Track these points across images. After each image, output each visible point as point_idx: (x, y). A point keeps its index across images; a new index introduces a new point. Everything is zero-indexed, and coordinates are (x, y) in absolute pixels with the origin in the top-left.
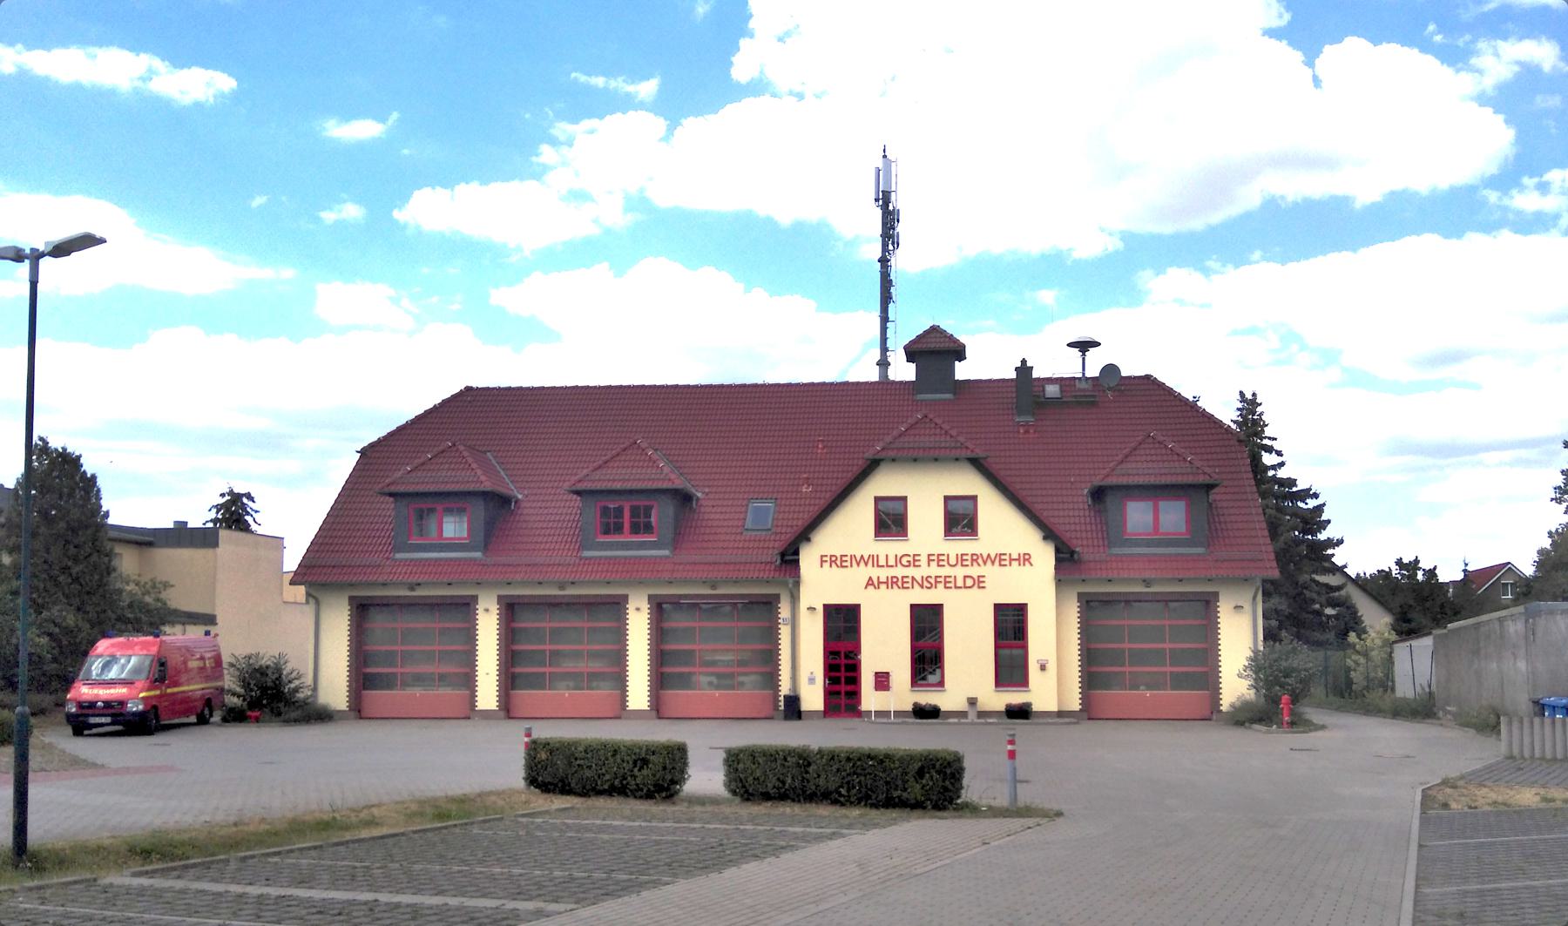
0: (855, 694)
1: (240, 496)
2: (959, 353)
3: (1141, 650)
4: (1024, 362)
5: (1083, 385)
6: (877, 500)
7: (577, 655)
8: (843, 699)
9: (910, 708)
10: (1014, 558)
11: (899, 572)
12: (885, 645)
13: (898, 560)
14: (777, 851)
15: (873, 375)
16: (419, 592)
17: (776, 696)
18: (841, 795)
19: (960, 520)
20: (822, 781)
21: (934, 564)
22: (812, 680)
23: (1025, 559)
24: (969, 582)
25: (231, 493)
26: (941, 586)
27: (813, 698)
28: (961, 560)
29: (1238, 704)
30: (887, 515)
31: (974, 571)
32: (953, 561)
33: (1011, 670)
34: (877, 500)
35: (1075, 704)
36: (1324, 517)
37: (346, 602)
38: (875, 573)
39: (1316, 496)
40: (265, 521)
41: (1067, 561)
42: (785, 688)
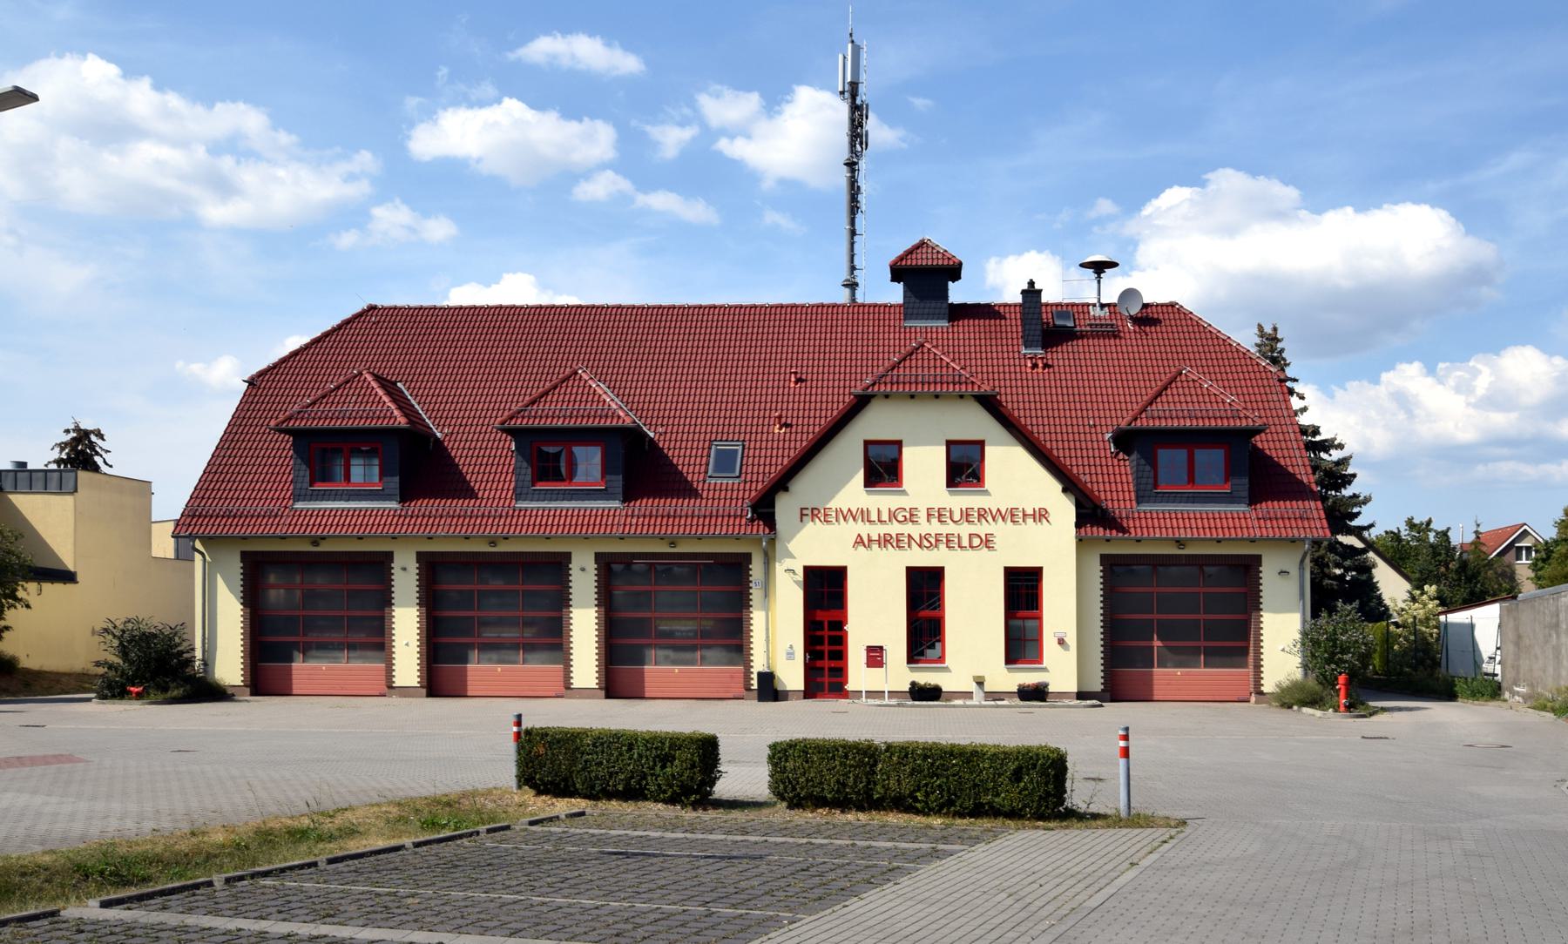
0: (840, 672)
1: (86, 433)
2: (954, 272)
3: (1166, 618)
4: (1031, 283)
5: (1097, 312)
6: (867, 443)
7: (500, 623)
8: (826, 679)
9: (906, 688)
10: (1028, 514)
11: (894, 529)
12: (875, 614)
13: (893, 515)
14: (889, 874)
15: (843, 297)
16: (503, 547)
17: (747, 673)
18: (916, 800)
19: (964, 468)
20: (892, 783)
21: (934, 521)
22: (790, 655)
23: (1041, 515)
24: (976, 542)
25: (77, 429)
26: (942, 546)
27: (792, 676)
28: (966, 515)
29: (1286, 683)
30: (880, 463)
31: (983, 529)
32: (957, 517)
33: (1021, 644)
34: (867, 443)
35: (1097, 685)
36: (1350, 471)
37: (238, 558)
38: (864, 529)
39: (1341, 446)
40: (119, 458)
41: (1090, 514)
42: (758, 664)
